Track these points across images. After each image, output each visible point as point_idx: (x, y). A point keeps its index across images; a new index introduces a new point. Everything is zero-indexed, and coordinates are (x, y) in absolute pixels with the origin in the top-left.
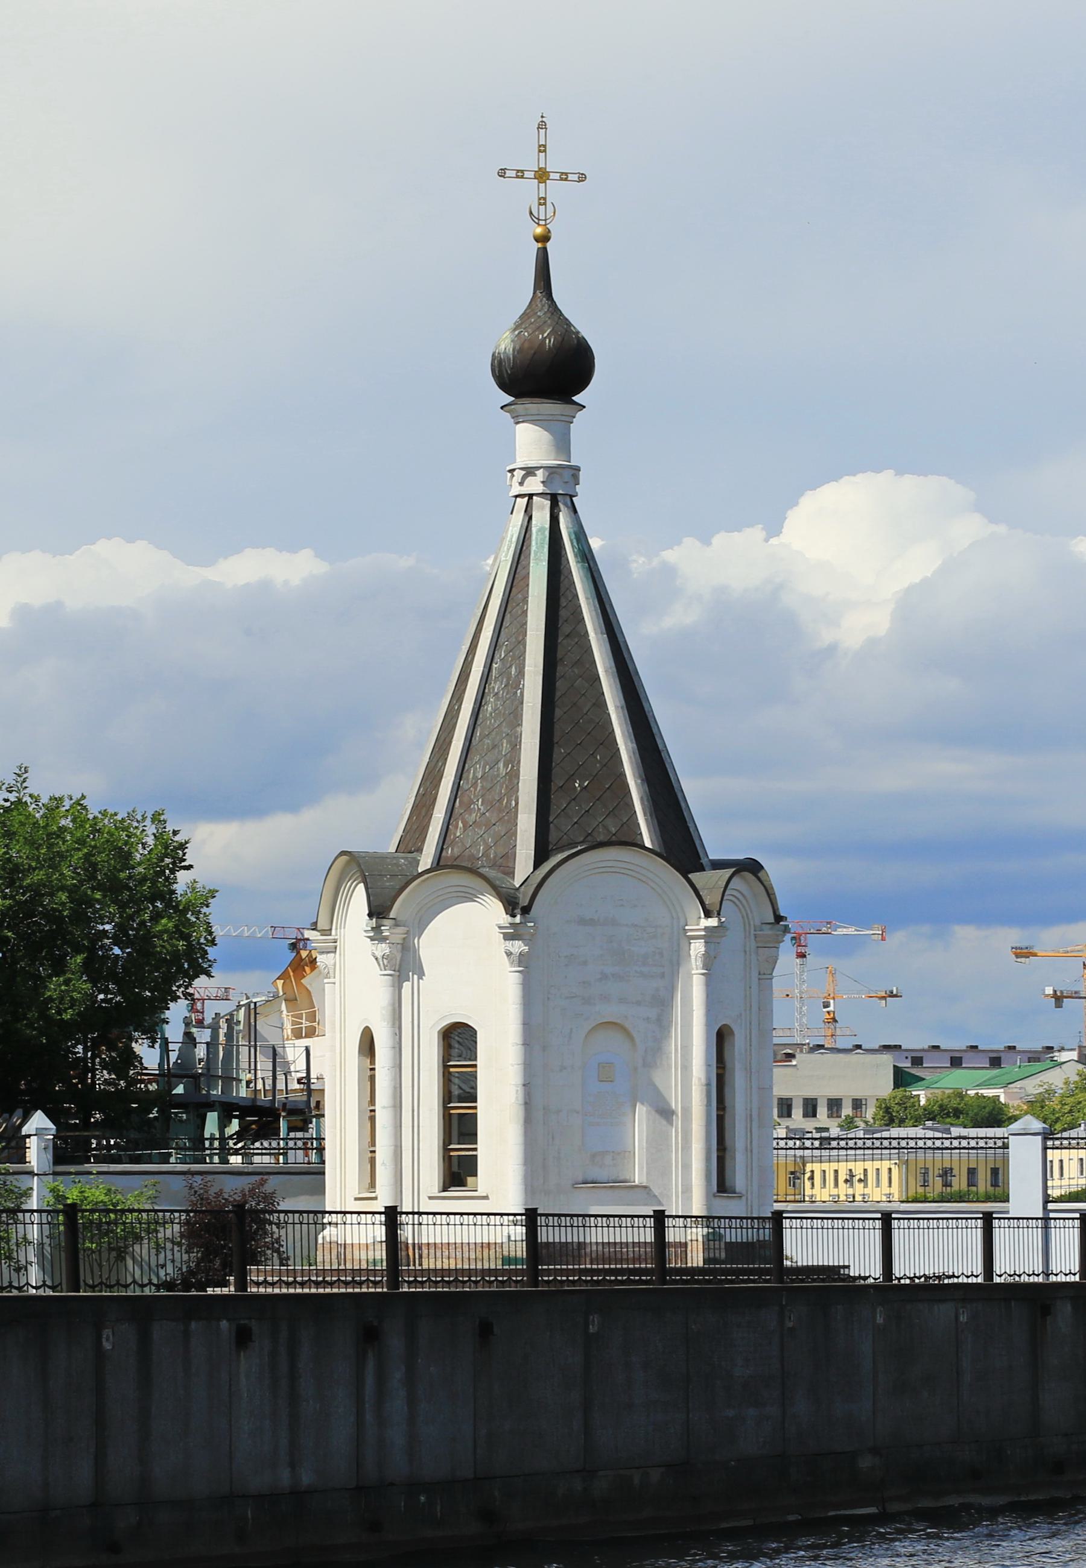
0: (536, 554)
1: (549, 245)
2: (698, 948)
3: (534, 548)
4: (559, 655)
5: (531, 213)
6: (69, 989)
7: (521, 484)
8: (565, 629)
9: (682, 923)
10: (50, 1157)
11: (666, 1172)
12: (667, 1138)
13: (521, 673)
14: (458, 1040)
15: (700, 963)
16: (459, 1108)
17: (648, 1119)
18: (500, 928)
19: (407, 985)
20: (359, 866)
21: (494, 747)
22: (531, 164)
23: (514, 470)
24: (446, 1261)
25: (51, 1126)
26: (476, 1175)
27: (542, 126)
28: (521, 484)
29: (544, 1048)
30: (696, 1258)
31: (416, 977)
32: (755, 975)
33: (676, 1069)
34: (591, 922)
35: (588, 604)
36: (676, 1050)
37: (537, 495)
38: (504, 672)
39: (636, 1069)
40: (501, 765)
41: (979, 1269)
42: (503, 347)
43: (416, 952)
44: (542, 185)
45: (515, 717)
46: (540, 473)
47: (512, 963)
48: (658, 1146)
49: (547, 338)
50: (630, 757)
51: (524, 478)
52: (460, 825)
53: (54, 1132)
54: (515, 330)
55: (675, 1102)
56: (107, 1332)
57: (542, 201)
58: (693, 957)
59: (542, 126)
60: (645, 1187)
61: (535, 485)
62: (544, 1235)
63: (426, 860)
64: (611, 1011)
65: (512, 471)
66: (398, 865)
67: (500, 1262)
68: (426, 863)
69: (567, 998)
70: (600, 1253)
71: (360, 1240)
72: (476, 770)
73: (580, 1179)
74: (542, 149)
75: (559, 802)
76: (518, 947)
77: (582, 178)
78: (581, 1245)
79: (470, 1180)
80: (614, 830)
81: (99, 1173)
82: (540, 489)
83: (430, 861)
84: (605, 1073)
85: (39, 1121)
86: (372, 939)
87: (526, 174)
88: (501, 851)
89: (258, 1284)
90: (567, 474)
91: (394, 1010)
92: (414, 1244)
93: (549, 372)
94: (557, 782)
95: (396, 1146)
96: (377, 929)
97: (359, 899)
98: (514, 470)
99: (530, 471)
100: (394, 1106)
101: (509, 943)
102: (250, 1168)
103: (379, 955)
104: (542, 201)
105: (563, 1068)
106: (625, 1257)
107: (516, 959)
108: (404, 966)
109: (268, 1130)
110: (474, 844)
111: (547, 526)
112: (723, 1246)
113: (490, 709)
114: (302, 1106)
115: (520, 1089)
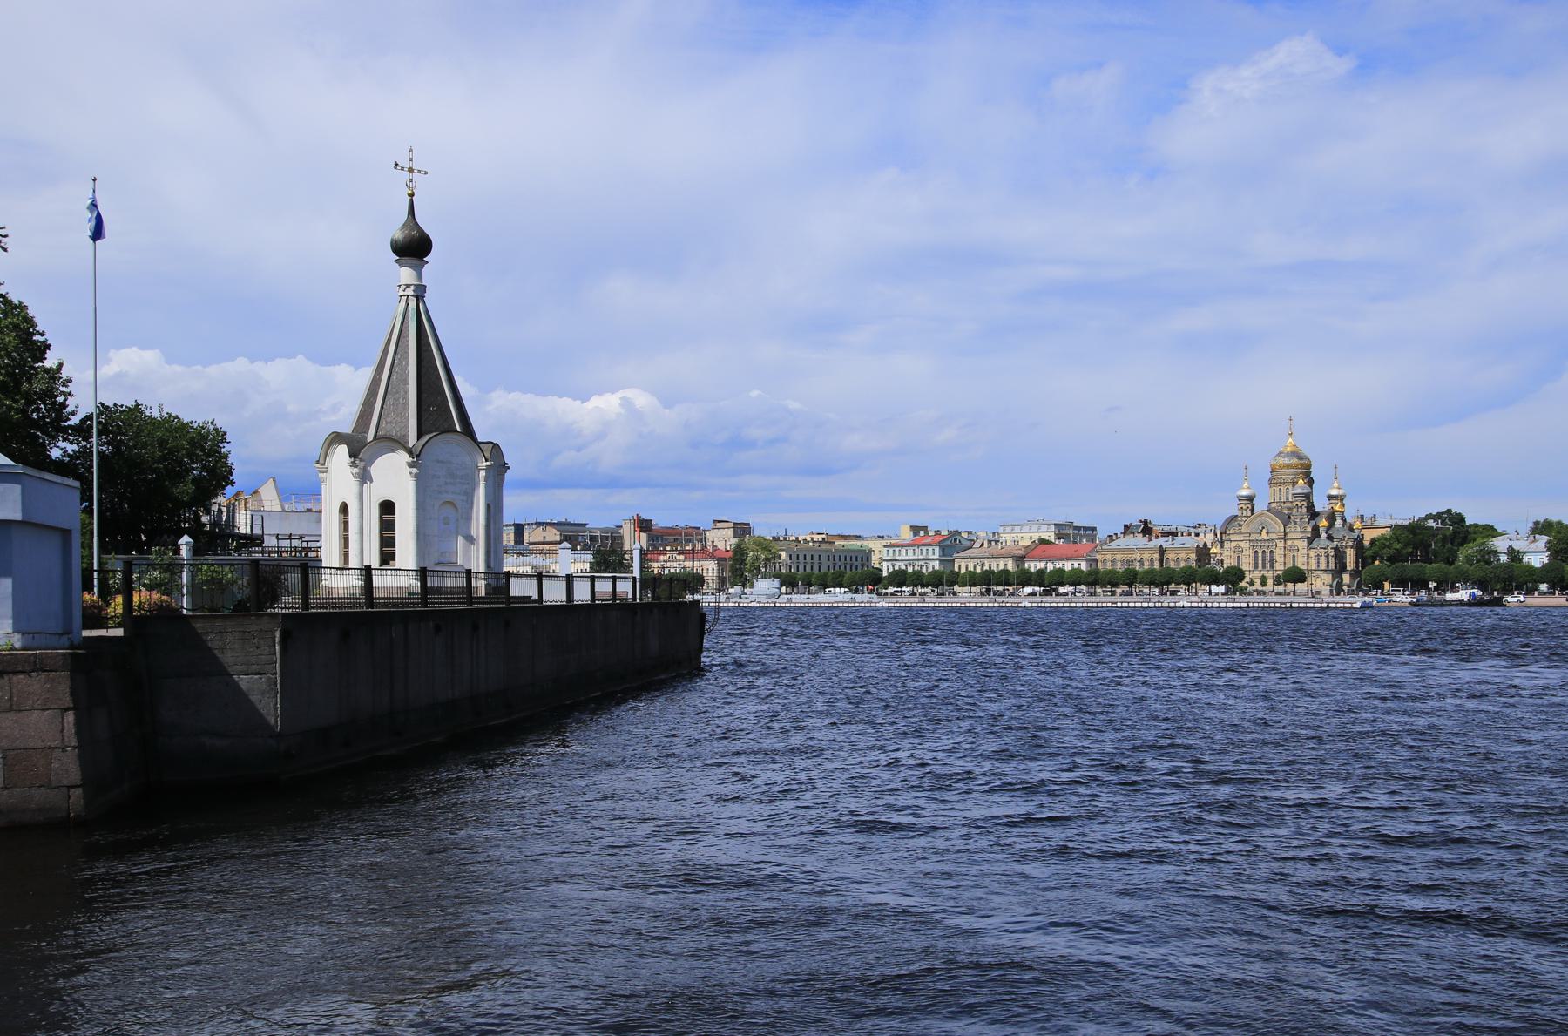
2: (483, 473)
6: (185, 489)
14: (387, 508)
16: (387, 534)
20: (337, 438)
30: (482, 593)
41: (588, 597)
45: (406, 382)
48: (467, 553)
55: (473, 533)
61: (410, 291)
63: (370, 438)
64: (449, 497)
72: (390, 400)
76: (415, 470)
84: (446, 521)
85: (186, 539)
93: (414, 248)
97: (342, 451)
99: (408, 286)
108: (364, 478)
109: (245, 545)
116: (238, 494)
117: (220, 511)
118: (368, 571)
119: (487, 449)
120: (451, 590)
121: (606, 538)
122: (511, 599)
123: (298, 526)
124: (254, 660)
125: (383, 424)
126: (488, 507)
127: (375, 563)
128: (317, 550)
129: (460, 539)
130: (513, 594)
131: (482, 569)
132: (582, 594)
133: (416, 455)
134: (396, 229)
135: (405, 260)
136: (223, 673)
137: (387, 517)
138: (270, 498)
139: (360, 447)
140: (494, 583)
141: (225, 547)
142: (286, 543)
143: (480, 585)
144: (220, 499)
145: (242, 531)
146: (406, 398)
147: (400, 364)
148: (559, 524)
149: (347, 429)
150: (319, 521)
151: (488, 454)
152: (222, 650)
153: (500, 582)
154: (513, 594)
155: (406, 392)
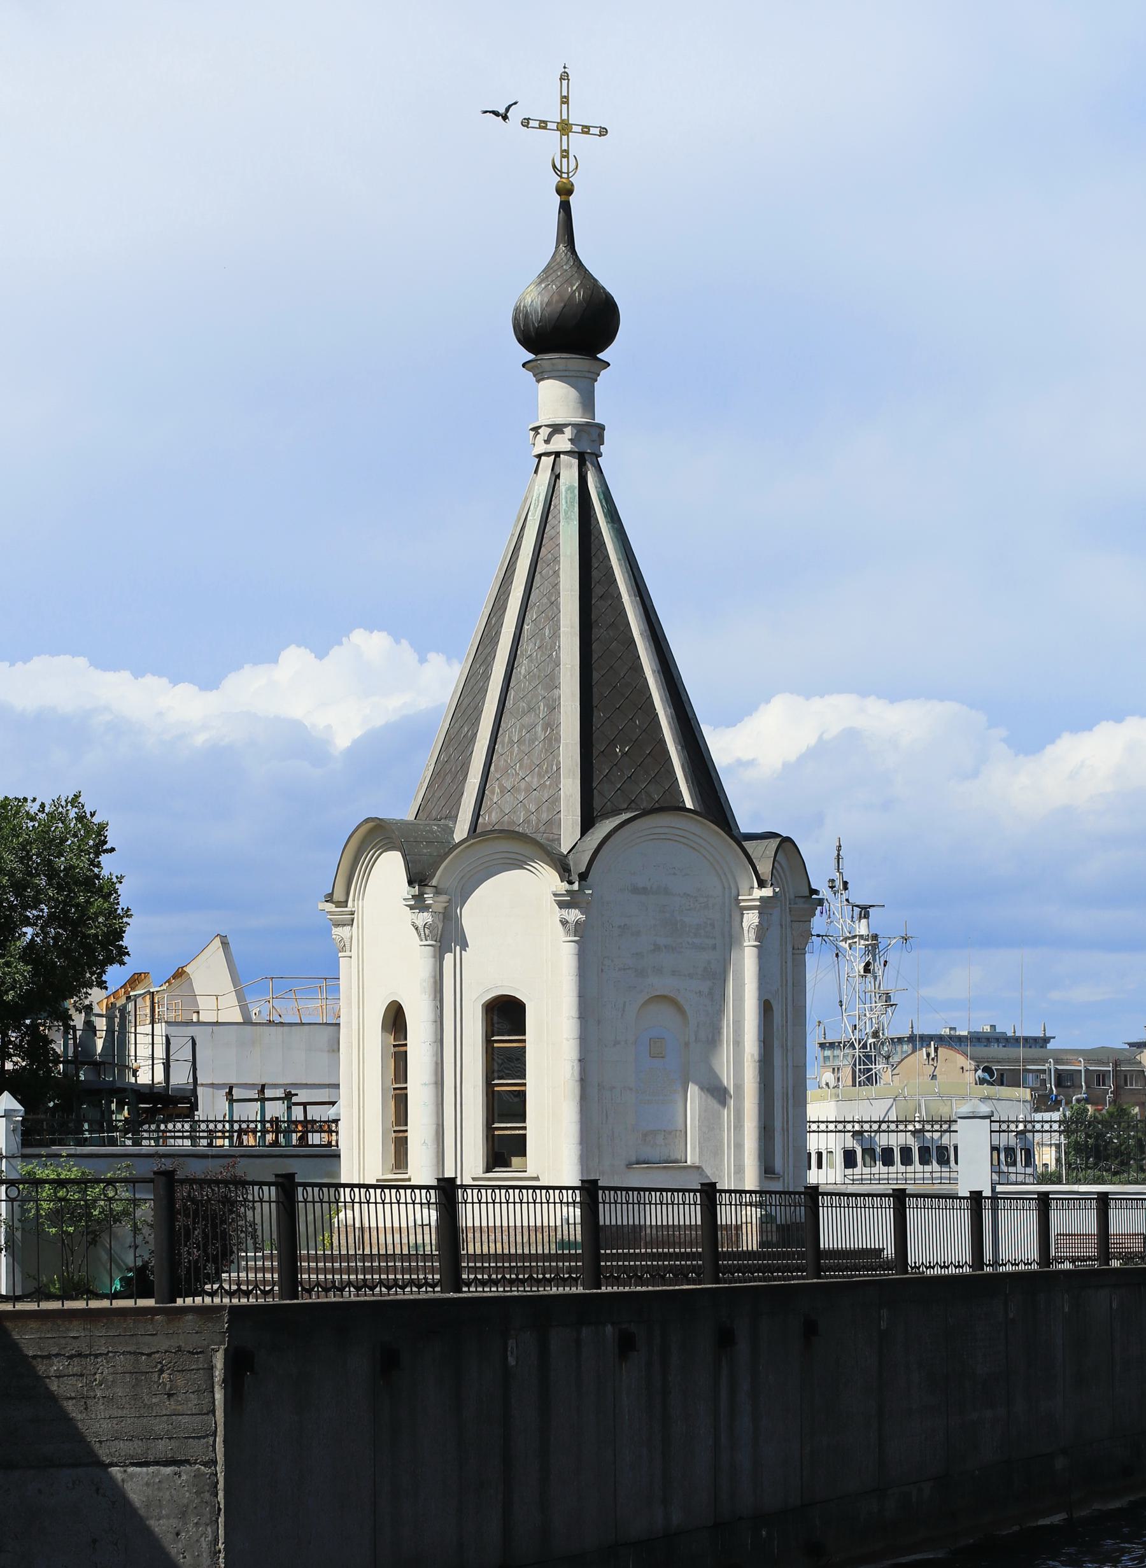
0: (566, 513)
1: (572, 199)
2: (751, 919)
3: (563, 506)
4: (593, 617)
5: (554, 167)
7: (547, 441)
8: (598, 591)
9: (734, 892)
10: (19, 1139)
11: (717, 1152)
12: (719, 1117)
13: (556, 634)
15: (752, 935)
16: (505, 1085)
17: (700, 1098)
18: (555, 895)
19: (449, 957)
20: (377, 835)
21: (530, 709)
22: (553, 115)
23: (540, 427)
24: (492, 1245)
25: (19, 1107)
26: (524, 1155)
27: (565, 77)
28: (547, 441)
29: (599, 1022)
30: (751, 1241)
31: (458, 948)
32: (790, 949)
33: (728, 1045)
34: (644, 891)
35: (620, 565)
36: (728, 1025)
37: (565, 453)
38: (538, 633)
39: (687, 1044)
40: (539, 728)
41: (966, 1256)
42: (529, 300)
43: (458, 921)
44: (565, 138)
45: (552, 682)
46: (568, 431)
47: (568, 933)
48: (710, 1127)
49: (574, 289)
50: (669, 723)
51: (551, 436)
52: (497, 790)
53: (22, 1113)
54: (540, 283)
56: (511, 1343)
57: (565, 154)
58: (746, 929)
59: (565, 77)
60: (698, 1168)
61: (562, 442)
62: (608, 1216)
63: (461, 831)
64: (662, 985)
65: (536, 430)
66: (433, 832)
67: (553, 1246)
68: (462, 830)
69: (620, 970)
70: (654, 1236)
71: (409, 1222)
73: (634, 1159)
74: (565, 100)
75: (601, 769)
76: (574, 915)
77: (603, 132)
78: (637, 1229)
79: (515, 1160)
80: (656, 797)
81: (69, 1156)
82: (568, 447)
83: (467, 827)
86: (412, 907)
87: (550, 126)
88: (545, 817)
89: (309, 1271)
90: (595, 432)
91: (435, 982)
92: (362, 1228)
93: (573, 330)
94: (599, 747)
95: (438, 1125)
96: (419, 899)
97: (389, 870)
98: (540, 427)
99: (557, 429)
100: (436, 1083)
101: (565, 912)
102: (214, 1151)
103: (420, 924)
104: (565, 154)
105: (616, 1043)
106: (677, 1240)
107: (572, 927)
108: (447, 937)
109: (150, 1116)
110: (514, 810)
111: (577, 485)
112: (774, 1229)
113: (523, 671)
114: (188, 1094)
115: (576, 1064)
116: (135, 980)
117: (90, 1027)
118: (447, 1192)
119: (764, 855)
120: (667, 1235)
121: (1101, 1077)
122: (819, 1258)
123: (275, 1063)
124: (161, 1427)
125: (494, 795)
126: (766, 1009)
127: (470, 1164)
128: (330, 1126)
129: (693, 1090)
130: (825, 1243)
131: (751, 1181)
132: (1016, 1244)
133: (580, 880)
134: (521, 278)
135: (552, 359)
136: (86, 1460)
137: (504, 1041)
138: (214, 992)
139: (439, 862)
140: (782, 1215)
141: (103, 1123)
142: (251, 1111)
143: (745, 1223)
144: (96, 996)
145: (144, 1078)
146: (552, 726)
147: (538, 633)
148: (977, 1039)
149: (403, 809)
150: (334, 1047)
151: (765, 868)
152: (84, 1399)
153: (795, 1208)
154: (825, 1243)
155: (554, 707)
